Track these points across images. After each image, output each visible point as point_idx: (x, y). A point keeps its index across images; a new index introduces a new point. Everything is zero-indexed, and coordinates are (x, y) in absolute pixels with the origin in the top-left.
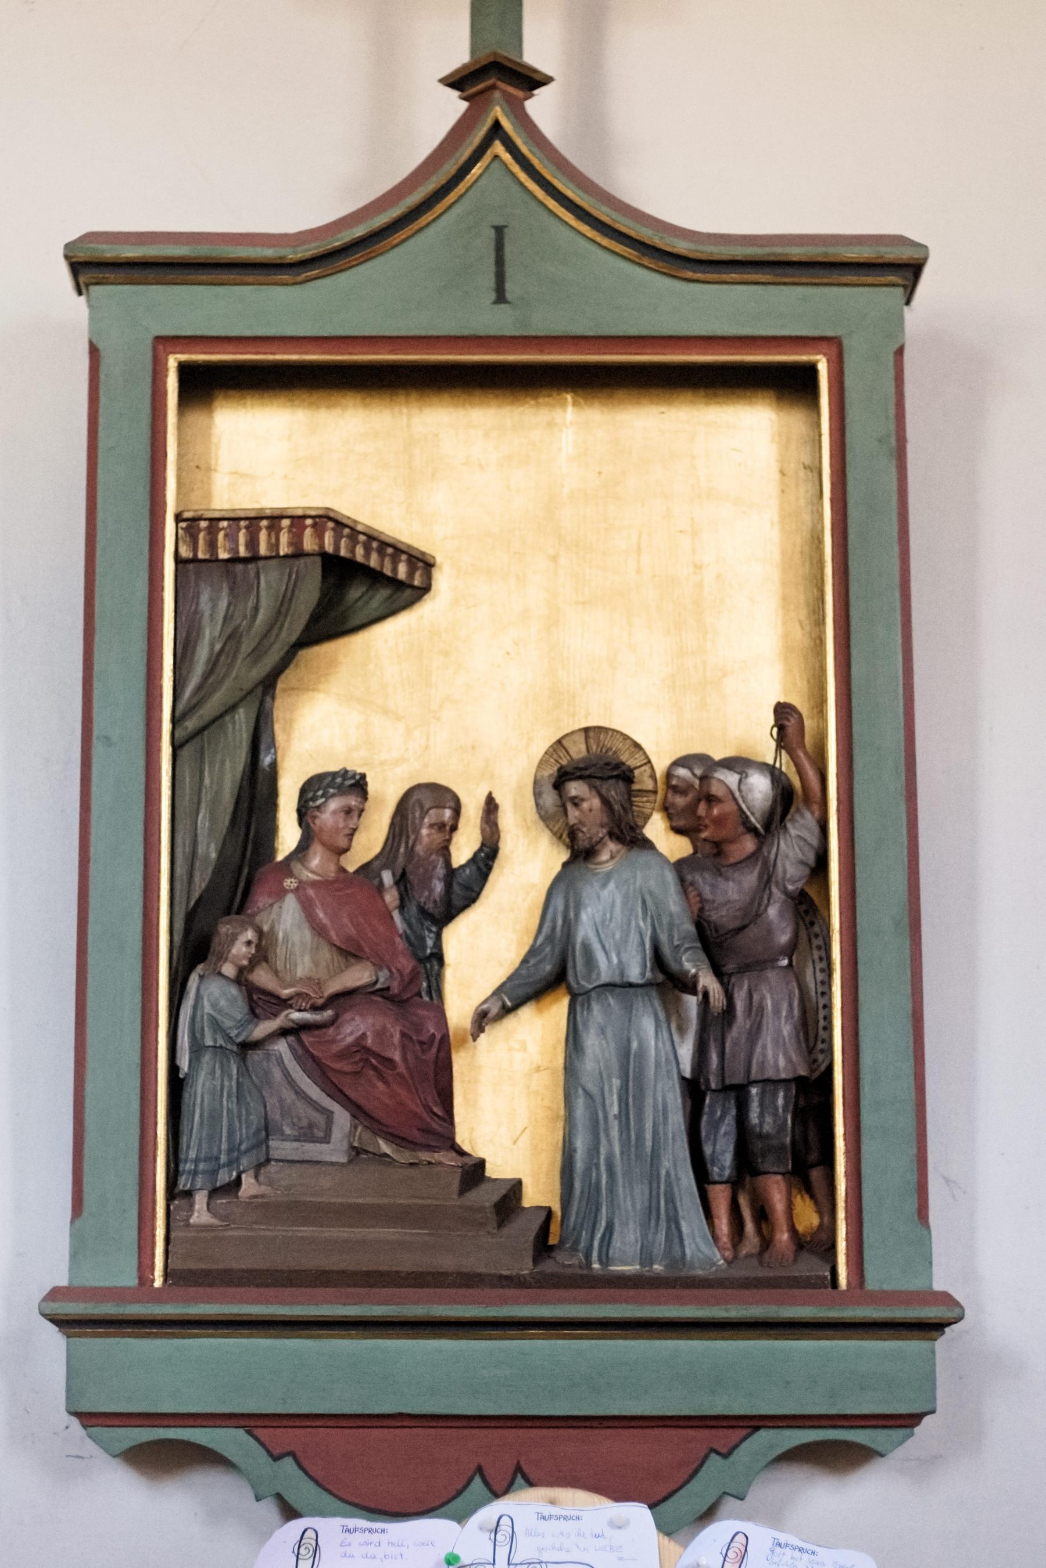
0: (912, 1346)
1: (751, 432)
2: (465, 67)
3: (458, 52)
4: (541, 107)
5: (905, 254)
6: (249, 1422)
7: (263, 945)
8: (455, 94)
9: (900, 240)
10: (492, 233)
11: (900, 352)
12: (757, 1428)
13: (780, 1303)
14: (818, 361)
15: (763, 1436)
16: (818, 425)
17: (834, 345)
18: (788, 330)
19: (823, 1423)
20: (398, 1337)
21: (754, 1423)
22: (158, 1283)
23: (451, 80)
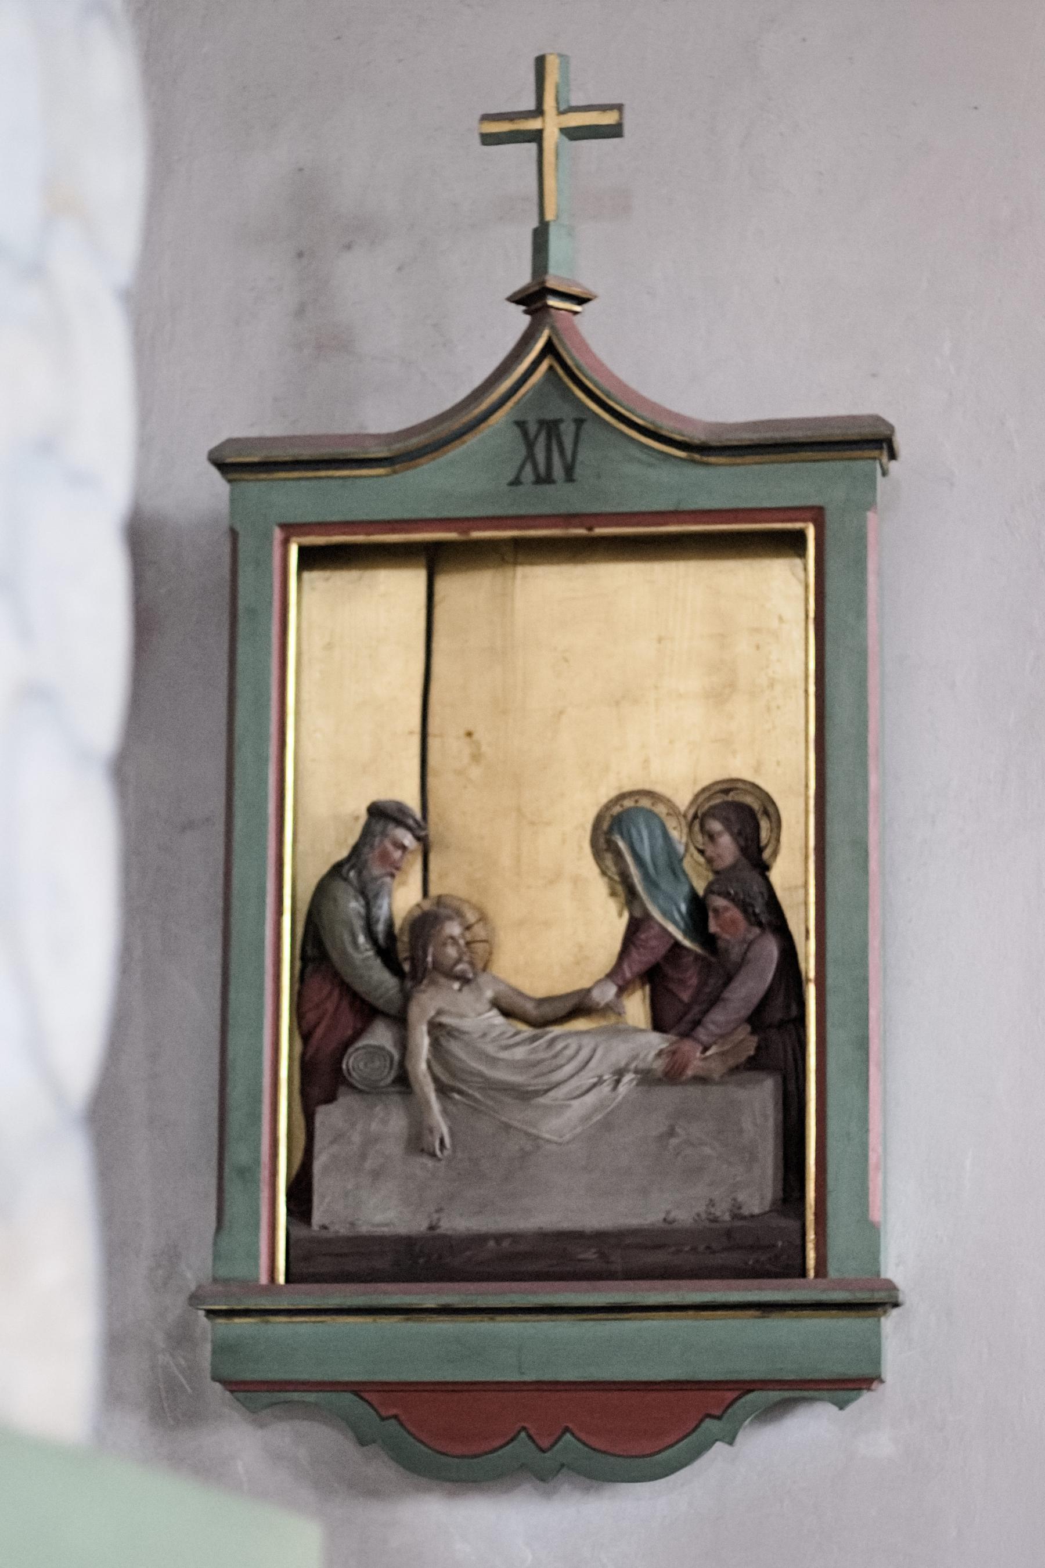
3: (522, 278)
8: (523, 308)
18: (788, 493)
22: (281, 1279)
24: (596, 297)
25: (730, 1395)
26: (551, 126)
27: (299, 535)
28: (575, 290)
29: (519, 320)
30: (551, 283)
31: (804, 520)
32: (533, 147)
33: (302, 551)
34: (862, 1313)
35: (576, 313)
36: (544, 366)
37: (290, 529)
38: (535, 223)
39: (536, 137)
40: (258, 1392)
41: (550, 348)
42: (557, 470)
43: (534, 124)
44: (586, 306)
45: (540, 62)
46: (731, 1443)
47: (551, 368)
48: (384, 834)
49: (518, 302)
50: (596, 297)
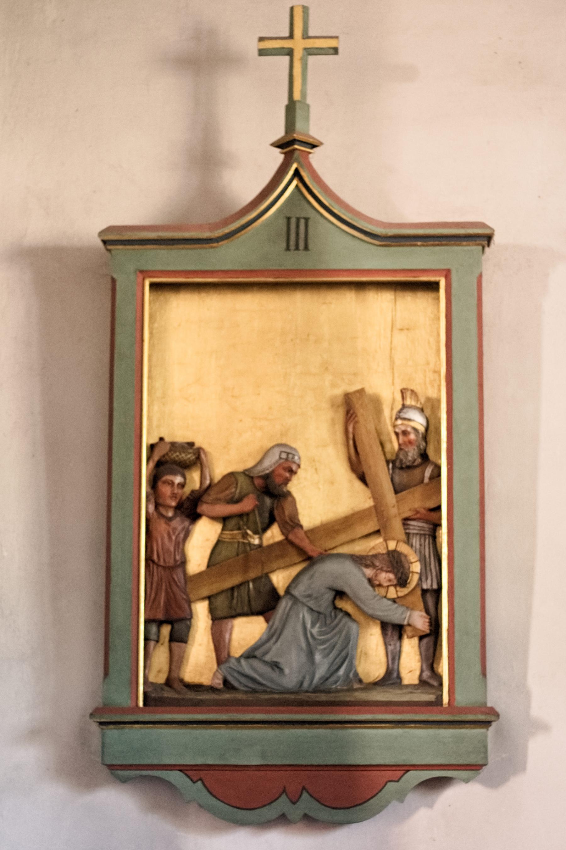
0: (477, 731)
1: (416, 306)
2: (283, 138)
3: (279, 133)
4: (316, 158)
5: (487, 231)
6: (183, 769)
7: (179, 540)
8: (278, 150)
9: (483, 225)
10: (285, 221)
11: (480, 276)
12: (408, 771)
13: (322, 713)
14: (439, 281)
15: (411, 773)
16: (438, 311)
17: (447, 274)
18: (435, 261)
19: (450, 768)
20: (161, 728)
21: (407, 768)
22: (141, 704)
23: (276, 145)
24: (321, 144)
25: (400, 773)
26: (298, 45)
27: (151, 277)
28: (311, 141)
29: (278, 157)
30: (296, 136)
31: (440, 276)
32: (287, 58)
33: (152, 285)
34: (295, 726)
35: (310, 153)
36: (295, 182)
37: (145, 273)
38: (285, 102)
39: (290, 53)
40: (122, 771)
41: (297, 174)
42: (284, 242)
43: (287, 44)
44: (315, 150)
45: (292, 9)
46: (402, 801)
47: (297, 186)
48: (405, 463)
49: (278, 147)
50: (321, 144)
